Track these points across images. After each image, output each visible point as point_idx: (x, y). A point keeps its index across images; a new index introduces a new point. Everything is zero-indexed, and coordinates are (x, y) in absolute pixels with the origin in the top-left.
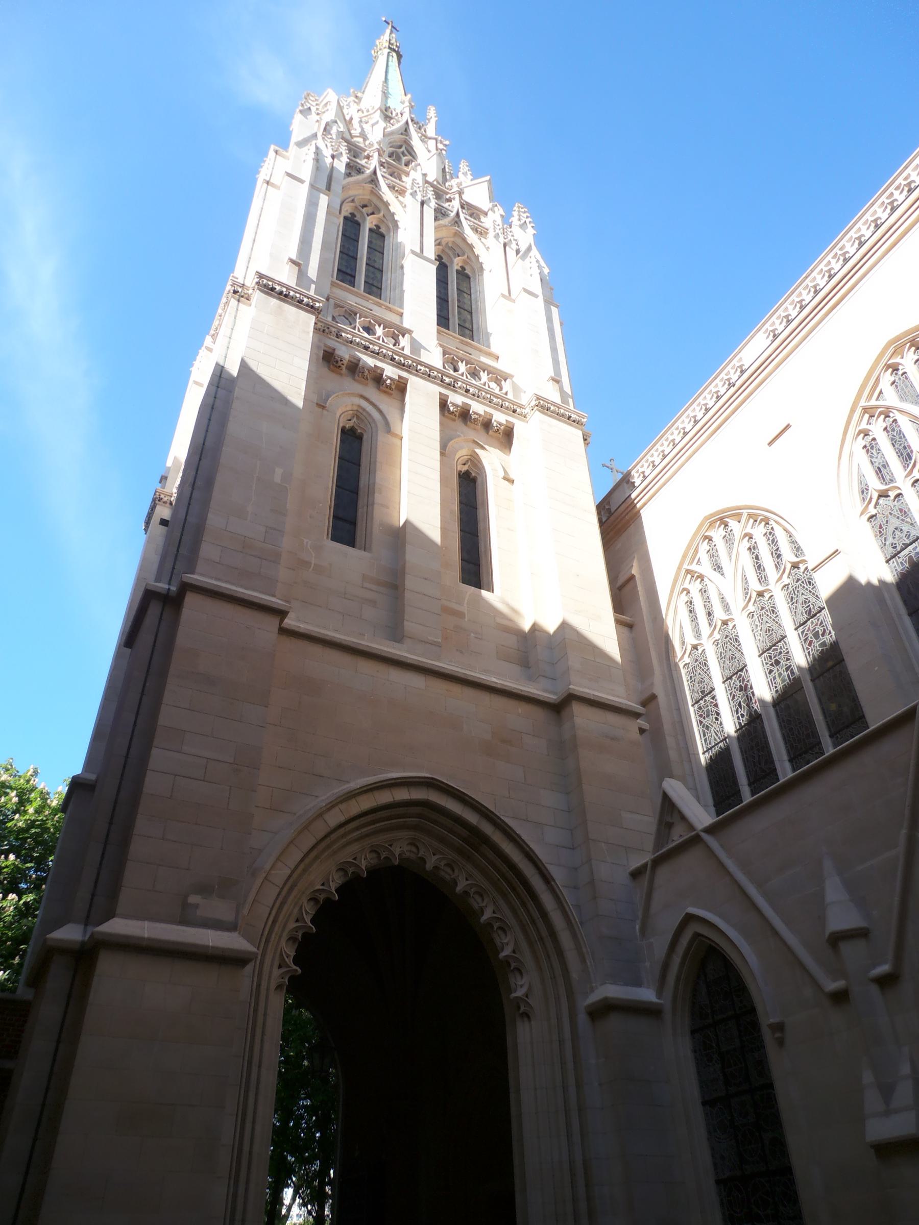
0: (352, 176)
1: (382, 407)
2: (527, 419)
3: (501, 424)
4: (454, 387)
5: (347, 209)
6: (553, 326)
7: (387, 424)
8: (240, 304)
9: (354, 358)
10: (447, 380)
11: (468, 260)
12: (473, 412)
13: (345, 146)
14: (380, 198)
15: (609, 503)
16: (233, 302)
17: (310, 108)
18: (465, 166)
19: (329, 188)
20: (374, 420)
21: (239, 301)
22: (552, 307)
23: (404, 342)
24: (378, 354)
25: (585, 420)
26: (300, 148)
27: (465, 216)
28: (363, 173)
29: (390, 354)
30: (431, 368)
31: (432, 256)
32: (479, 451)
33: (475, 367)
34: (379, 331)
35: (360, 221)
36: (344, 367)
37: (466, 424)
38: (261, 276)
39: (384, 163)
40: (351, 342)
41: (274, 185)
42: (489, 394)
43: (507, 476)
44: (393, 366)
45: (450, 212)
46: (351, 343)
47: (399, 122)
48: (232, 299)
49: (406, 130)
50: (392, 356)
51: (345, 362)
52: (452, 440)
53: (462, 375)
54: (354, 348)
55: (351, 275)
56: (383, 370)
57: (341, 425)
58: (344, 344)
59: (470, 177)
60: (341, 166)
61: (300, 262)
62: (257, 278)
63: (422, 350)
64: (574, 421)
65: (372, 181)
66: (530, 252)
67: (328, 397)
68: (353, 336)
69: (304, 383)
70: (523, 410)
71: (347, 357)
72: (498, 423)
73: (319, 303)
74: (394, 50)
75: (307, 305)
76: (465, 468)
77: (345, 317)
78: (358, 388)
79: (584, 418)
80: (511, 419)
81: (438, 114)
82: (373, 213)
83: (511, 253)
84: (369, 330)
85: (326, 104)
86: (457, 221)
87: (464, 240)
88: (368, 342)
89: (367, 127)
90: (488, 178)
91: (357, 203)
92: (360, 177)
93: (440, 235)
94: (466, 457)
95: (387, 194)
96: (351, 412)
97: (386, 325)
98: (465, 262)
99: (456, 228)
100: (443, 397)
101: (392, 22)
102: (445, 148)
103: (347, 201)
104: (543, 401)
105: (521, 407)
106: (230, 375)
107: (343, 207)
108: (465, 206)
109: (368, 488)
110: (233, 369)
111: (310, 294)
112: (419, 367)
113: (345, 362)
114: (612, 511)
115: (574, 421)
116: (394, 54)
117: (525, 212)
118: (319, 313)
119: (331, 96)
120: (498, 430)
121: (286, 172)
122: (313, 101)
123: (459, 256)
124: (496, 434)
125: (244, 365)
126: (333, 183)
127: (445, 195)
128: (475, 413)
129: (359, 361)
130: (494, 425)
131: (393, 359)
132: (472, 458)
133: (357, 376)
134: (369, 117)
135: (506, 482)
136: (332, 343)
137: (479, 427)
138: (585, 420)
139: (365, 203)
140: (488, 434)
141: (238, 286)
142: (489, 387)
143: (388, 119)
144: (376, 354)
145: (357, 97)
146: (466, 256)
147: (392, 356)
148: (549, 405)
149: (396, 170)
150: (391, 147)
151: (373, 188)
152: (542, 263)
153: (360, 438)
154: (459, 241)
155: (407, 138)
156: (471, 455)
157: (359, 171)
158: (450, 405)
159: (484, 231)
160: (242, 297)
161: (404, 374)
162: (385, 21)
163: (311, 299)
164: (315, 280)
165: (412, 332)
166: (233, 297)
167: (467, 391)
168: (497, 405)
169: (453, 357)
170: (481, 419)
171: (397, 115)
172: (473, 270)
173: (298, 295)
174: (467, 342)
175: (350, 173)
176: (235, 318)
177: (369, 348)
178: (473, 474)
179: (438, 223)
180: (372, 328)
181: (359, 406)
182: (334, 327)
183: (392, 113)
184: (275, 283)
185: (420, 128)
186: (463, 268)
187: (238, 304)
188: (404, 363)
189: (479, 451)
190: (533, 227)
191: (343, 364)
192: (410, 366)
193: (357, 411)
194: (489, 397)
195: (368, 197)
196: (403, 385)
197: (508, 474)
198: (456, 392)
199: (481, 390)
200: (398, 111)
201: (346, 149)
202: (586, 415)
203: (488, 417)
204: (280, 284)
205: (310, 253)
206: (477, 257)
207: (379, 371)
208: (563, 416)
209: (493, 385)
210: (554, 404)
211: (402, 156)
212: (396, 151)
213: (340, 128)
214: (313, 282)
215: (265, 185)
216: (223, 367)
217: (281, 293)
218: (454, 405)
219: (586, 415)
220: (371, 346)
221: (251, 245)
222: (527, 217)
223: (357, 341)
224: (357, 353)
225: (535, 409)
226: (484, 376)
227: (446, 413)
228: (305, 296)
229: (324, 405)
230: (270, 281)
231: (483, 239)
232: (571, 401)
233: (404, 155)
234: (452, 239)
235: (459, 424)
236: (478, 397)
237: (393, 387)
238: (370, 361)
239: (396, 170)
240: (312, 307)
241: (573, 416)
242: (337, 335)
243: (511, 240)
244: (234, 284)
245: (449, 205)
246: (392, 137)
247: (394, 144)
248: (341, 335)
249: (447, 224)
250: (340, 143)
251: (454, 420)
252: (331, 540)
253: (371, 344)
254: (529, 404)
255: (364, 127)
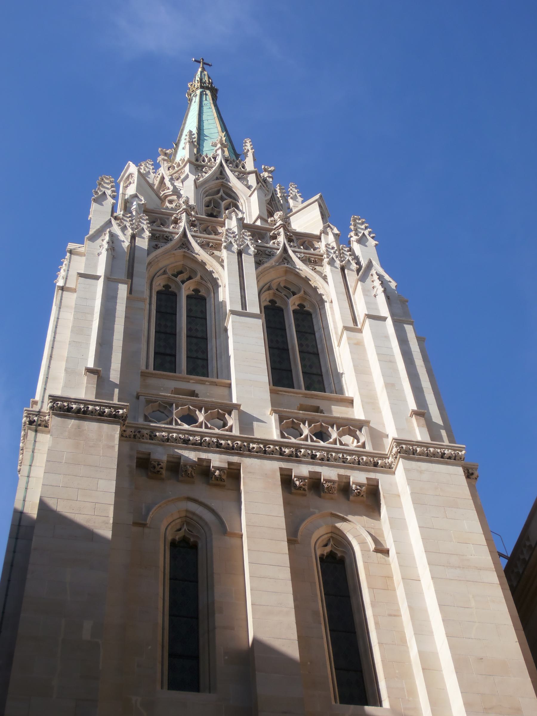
0: (159, 248)
1: (213, 504)
2: (393, 470)
3: (361, 485)
4: (297, 456)
5: (159, 284)
6: (409, 348)
7: (222, 523)
8: (38, 434)
9: (173, 457)
10: (287, 451)
11: (305, 296)
12: (324, 480)
13: (147, 220)
14: (195, 260)
15: (528, 539)
16: (31, 434)
17: (104, 193)
18: (294, 189)
19: (130, 274)
20: (206, 523)
21: (36, 431)
22: (405, 326)
23: (232, 420)
24: (201, 444)
25: (464, 452)
26: (93, 242)
27: (293, 249)
28: (171, 240)
29: (215, 440)
30: (266, 442)
31: (257, 310)
32: (339, 525)
33: (321, 425)
34: (201, 417)
35: (176, 291)
36: (164, 472)
37: (320, 496)
38: (54, 399)
39: (194, 221)
40: (168, 440)
41: (70, 290)
42: (340, 453)
43: (379, 547)
44: (221, 453)
45: (275, 251)
46: (168, 442)
47: (212, 168)
48: (29, 431)
49: (221, 173)
50: (218, 442)
51: (164, 465)
52: (303, 520)
53: (306, 439)
54: (173, 446)
55: (170, 355)
56: (209, 461)
57: (169, 538)
58: (160, 445)
59: (300, 199)
60: (143, 243)
61: (98, 369)
62: (51, 402)
63: (255, 423)
64: (450, 458)
65: (183, 244)
66: (371, 269)
67: (148, 511)
68: (169, 432)
69: (112, 508)
70: (387, 461)
71: (165, 458)
72: (357, 484)
73: (122, 409)
74: (207, 88)
75: (110, 415)
76: (328, 549)
77: (160, 411)
78: (184, 490)
79: (461, 451)
80: (372, 475)
81: (254, 146)
82: (190, 278)
83: (352, 277)
84: (190, 419)
85: (129, 176)
86: (285, 258)
87: (298, 275)
88: (187, 434)
89: (178, 184)
90: (317, 197)
91: (170, 273)
92: (169, 245)
93: (266, 279)
94: (326, 536)
95: (202, 254)
96: (179, 520)
97: (207, 407)
98: (302, 298)
99: (286, 265)
100: (285, 473)
101: (203, 60)
102: (270, 175)
103: (158, 274)
104: (405, 444)
105: (384, 457)
106: (29, 518)
107: (154, 283)
108: (294, 238)
109: (208, 608)
110: (32, 511)
111: (114, 402)
112: (251, 445)
113: (164, 465)
114: (533, 546)
115: (450, 458)
116: (208, 92)
117: (363, 223)
118: (124, 420)
119: (132, 168)
120: (359, 493)
121: (78, 274)
122: (108, 184)
123: (294, 294)
124: (360, 498)
125: (43, 506)
126: (136, 265)
127: (268, 233)
128: (327, 481)
129: (180, 458)
130: (354, 488)
131: (219, 445)
132: (334, 536)
133: (180, 476)
134: (180, 172)
135: (379, 555)
136: (145, 447)
137: (336, 494)
138: (464, 452)
139: (180, 269)
140: (348, 499)
141: (33, 414)
142: (341, 444)
143: (200, 168)
144: (199, 446)
145: (166, 154)
146: (302, 292)
147: (218, 442)
148: (414, 447)
149: (209, 224)
150: (206, 196)
151: (184, 252)
152: (387, 277)
153: (194, 547)
154: (291, 278)
155: (223, 180)
156: (331, 532)
157: (167, 239)
158: (295, 479)
159: (318, 259)
160: (40, 425)
161: (235, 459)
162: (195, 61)
163: (113, 407)
164: (117, 382)
165: (240, 405)
166: (30, 429)
167: (314, 457)
168: (353, 463)
169: (293, 421)
170: (336, 485)
171: (210, 160)
172: (313, 306)
173: (98, 408)
174: (312, 395)
175: (156, 245)
176: (33, 452)
177: (189, 440)
178: (339, 554)
179: (261, 268)
180: (192, 415)
181: (187, 511)
182: (146, 429)
183: (204, 161)
184: (71, 402)
185: (237, 166)
186: (301, 306)
187: (36, 435)
188: (233, 446)
189: (340, 525)
190: (373, 238)
191: (162, 468)
192: (241, 448)
193: (186, 516)
194: (341, 456)
195: (182, 263)
196: (236, 471)
197: (381, 544)
198: (300, 462)
199: (330, 451)
200: (210, 155)
201: (147, 223)
202: (464, 446)
203: (345, 480)
204: (78, 401)
205: (111, 354)
206: (315, 289)
207: (205, 464)
208: (434, 455)
209: (348, 439)
210: (420, 444)
211: (220, 201)
212: (213, 198)
213: (141, 200)
214: (115, 385)
215: (60, 291)
216: (22, 513)
217: (79, 411)
218: (299, 478)
219: (464, 446)
220: (191, 438)
221: (54, 353)
222: (366, 228)
223: (174, 436)
224: (176, 450)
225: (398, 456)
226: (334, 434)
227: (293, 490)
228: (106, 407)
229: (143, 522)
230: (65, 401)
231: (317, 268)
232: (443, 433)
233: (222, 199)
234: (284, 278)
235: (312, 499)
236: (328, 460)
237: (224, 477)
238: (192, 455)
239: (209, 224)
240: (115, 416)
241: (446, 452)
242: (150, 436)
243: (349, 260)
244: (29, 414)
245: (274, 243)
246: (207, 185)
247: (210, 191)
248: (156, 435)
249: (274, 264)
250: (141, 218)
251: (304, 495)
252: (169, 689)
253: (191, 435)
254: (391, 452)
255: (175, 184)
